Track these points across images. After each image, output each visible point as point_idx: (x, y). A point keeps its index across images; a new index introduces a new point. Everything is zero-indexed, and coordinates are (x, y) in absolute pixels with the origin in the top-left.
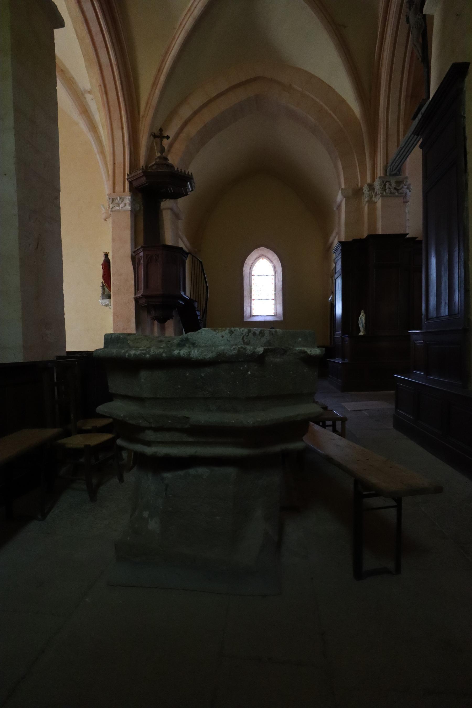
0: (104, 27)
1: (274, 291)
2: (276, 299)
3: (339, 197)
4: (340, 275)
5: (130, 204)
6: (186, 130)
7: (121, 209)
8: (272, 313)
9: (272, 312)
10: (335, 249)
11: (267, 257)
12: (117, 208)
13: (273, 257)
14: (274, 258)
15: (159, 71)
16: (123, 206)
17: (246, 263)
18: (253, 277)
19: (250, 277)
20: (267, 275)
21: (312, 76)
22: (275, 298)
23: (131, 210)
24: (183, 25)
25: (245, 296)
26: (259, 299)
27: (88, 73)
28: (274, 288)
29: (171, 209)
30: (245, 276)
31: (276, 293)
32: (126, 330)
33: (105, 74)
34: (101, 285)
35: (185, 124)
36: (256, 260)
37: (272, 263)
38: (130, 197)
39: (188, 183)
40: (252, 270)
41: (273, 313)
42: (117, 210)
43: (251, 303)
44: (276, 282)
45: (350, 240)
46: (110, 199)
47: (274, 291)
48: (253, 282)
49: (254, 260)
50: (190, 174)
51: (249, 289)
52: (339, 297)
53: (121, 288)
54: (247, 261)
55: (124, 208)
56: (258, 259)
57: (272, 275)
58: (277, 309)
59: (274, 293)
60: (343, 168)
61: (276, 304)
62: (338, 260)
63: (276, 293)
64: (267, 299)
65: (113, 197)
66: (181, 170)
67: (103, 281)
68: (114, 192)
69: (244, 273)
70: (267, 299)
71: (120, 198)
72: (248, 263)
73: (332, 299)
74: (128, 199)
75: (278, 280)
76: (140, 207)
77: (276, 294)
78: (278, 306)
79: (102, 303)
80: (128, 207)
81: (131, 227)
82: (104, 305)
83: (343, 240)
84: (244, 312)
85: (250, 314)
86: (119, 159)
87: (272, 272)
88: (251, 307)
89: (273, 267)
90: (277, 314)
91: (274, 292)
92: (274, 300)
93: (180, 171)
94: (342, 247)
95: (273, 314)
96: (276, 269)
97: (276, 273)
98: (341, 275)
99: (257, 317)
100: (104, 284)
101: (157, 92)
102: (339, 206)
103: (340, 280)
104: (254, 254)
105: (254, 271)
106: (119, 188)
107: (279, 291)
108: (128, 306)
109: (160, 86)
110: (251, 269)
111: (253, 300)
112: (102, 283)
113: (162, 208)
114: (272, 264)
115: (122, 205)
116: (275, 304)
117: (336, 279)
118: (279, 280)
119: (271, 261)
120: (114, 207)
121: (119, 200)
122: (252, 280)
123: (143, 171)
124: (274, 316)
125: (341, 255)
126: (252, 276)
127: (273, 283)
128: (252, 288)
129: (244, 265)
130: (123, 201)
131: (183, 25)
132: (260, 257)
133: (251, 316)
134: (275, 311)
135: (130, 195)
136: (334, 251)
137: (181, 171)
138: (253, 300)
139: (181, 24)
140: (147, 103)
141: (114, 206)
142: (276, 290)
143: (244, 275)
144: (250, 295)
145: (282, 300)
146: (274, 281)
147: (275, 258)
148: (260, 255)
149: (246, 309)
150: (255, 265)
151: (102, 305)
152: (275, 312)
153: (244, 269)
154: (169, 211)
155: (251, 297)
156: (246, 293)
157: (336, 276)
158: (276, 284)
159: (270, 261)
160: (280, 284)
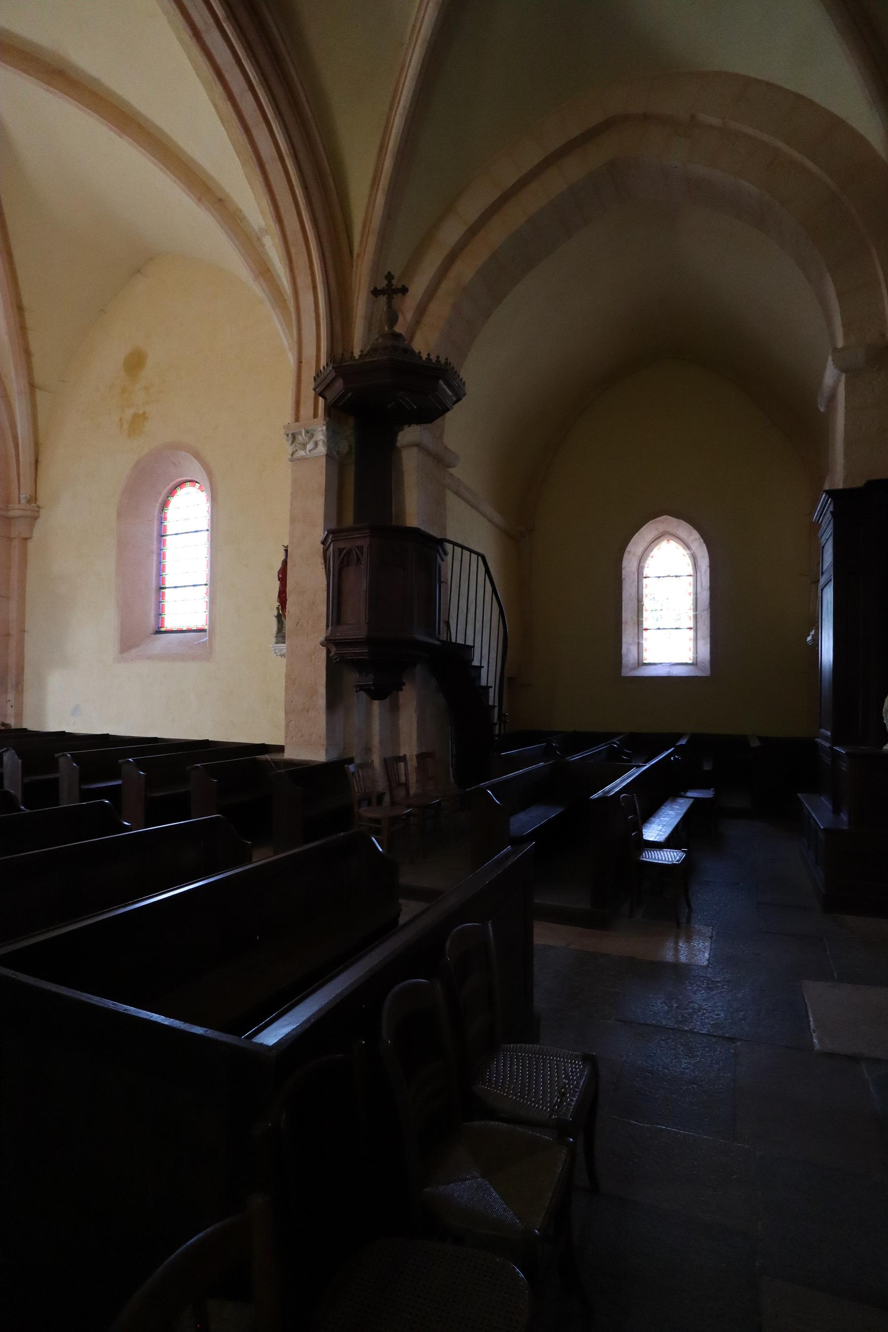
0: (254, 77)
1: (693, 609)
2: (696, 629)
3: (831, 375)
4: (830, 580)
5: (326, 441)
6: (452, 274)
7: (308, 453)
8: (688, 657)
9: (687, 657)
10: (819, 510)
11: (678, 538)
12: (301, 453)
13: (690, 536)
14: (692, 538)
15: (382, 148)
16: (311, 448)
17: (629, 552)
18: (645, 581)
19: (638, 581)
20: (676, 576)
21: (748, 82)
22: (694, 626)
23: (327, 455)
24: (417, 29)
25: (625, 621)
26: (659, 629)
27: (252, 188)
28: (693, 604)
29: (418, 445)
30: (627, 580)
31: (696, 615)
32: (308, 712)
33: (271, 178)
34: (275, 613)
35: (452, 258)
36: (653, 544)
37: (689, 550)
38: (324, 428)
39: (441, 382)
40: (644, 566)
41: (690, 659)
42: (302, 456)
43: (640, 637)
44: (698, 589)
45: (860, 483)
46: (287, 435)
47: (692, 611)
48: (645, 591)
49: (646, 544)
50: (443, 361)
51: (636, 606)
52: (829, 640)
53: (302, 621)
54: (631, 547)
55: (315, 452)
56: (657, 541)
57: (688, 576)
58: (698, 650)
59: (694, 615)
60: (840, 295)
61: (696, 639)
62: (827, 540)
63: (696, 615)
64: (677, 628)
65: (294, 431)
66: (438, 357)
67: (279, 605)
68: (297, 419)
69: (623, 572)
70: (677, 628)
71: (307, 432)
72: (632, 552)
73: (813, 639)
74: (321, 433)
75: (702, 584)
76: (350, 447)
77: (696, 617)
78: (701, 643)
79: (276, 651)
80: (322, 449)
81: (327, 490)
82: (278, 654)
83: (840, 486)
84: (623, 656)
85: (637, 662)
86: (310, 351)
87: (690, 570)
88: (639, 645)
89: (689, 557)
90: (699, 660)
91: (694, 611)
92: (692, 630)
93: (434, 361)
94: (834, 507)
95: (690, 662)
96: (697, 562)
97: (696, 572)
98: (832, 582)
99: (653, 667)
100: (281, 612)
101: (380, 199)
102: (833, 397)
103: (830, 592)
104: (647, 532)
105: (648, 567)
106: (307, 410)
107: (704, 610)
108: (313, 661)
109: (384, 182)
110: (641, 564)
111: (646, 629)
112: (278, 608)
113: (398, 444)
114: (689, 552)
115: (309, 446)
116: (693, 639)
117: (822, 590)
118: (704, 585)
119: (687, 546)
120: (297, 450)
121: (305, 435)
122: (644, 586)
123: (335, 365)
124: (692, 664)
125: (831, 525)
126: (644, 579)
127: (690, 594)
128: (643, 605)
129: (625, 556)
130: (312, 436)
131: (417, 29)
132: (663, 538)
133: (641, 664)
134: (693, 654)
135: (325, 423)
136: (817, 515)
137: (438, 361)
138: (645, 629)
139: (414, 26)
140: (364, 227)
141: (295, 450)
142: (696, 608)
143: (623, 577)
144: (638, 620)
145: (709, 629)
146: (694, 587)
147: (694, 538)
148: (662, 533)
149: (628, 649)
150: (651, 555)
151: (275, 655)
152: (693, 657)
153: (625, 563)
154: (416, 449)
155: (639, 623)
156: (627, 614)
157: (822, 581)
158: (696, 594)
159: (684, 545)
160: (705, 595)
